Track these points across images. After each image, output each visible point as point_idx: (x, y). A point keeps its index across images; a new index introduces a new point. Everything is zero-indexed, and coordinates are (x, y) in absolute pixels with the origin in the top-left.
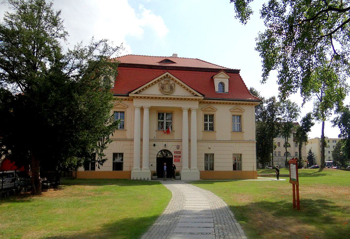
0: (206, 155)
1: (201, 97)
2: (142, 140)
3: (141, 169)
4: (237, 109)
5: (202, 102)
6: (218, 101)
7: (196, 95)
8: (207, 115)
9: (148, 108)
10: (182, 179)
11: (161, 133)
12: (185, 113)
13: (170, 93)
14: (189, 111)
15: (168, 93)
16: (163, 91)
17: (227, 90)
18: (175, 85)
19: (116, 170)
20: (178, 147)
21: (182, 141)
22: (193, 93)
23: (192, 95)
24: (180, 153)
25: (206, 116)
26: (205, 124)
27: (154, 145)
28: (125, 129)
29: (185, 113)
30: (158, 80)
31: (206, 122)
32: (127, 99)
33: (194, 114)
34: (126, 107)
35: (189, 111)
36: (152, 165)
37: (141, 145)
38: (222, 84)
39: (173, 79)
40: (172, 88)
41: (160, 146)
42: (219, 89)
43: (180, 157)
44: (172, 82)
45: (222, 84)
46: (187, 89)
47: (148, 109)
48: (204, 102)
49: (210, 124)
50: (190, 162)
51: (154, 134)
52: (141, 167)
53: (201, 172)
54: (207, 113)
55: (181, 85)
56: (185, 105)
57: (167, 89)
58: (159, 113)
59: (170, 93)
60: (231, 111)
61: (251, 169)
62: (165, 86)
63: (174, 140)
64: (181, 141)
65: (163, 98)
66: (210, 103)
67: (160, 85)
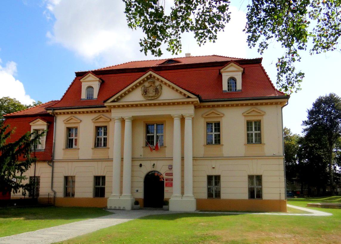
0: (210, 178)
1: (196, 100)
4: (212, 114)
6: (246, 101)
7: (189, 97)
8: (252, 122)
9: (129, 119)
11: (148, 149)
12: (177, 123)
13: (156, 98)
14: (183, 119)
15: (153, 98)
16: (146, 96)
17: (239, 87)
18: (162, 87)
19: (100, 197)
20: (171, 167)
21: (172, 160)
22: (185, 95)
23: (182, 97)
27: (141, 165)
28: (221, 144)
29: (177, 123)
30: (140, 83)
33: (188, 123)
34: (79, 121)
35: (183, 119)
36: (137, 191)
37: (122, 166)
38: (233, 79)
39: (158, 79)
40: (157, 91)
41: (148, 168)
42: (228, 86)
45: (232, 80)
46: (177, 90)
47: (191, 119)
48: (204, 107)
50: (183, 187)
51: (202, 151)
52: (121, 193)
54: (250, 119)
55: (169, 86)
56: (175, 112)
57: (151, 92)
58: (146, 124)
59: (156, 98)
60: (244, 116)
61: (276, 197)
62: (148, 90)
64: (171, 159)
65: (146, 105)
66: (213, 106)
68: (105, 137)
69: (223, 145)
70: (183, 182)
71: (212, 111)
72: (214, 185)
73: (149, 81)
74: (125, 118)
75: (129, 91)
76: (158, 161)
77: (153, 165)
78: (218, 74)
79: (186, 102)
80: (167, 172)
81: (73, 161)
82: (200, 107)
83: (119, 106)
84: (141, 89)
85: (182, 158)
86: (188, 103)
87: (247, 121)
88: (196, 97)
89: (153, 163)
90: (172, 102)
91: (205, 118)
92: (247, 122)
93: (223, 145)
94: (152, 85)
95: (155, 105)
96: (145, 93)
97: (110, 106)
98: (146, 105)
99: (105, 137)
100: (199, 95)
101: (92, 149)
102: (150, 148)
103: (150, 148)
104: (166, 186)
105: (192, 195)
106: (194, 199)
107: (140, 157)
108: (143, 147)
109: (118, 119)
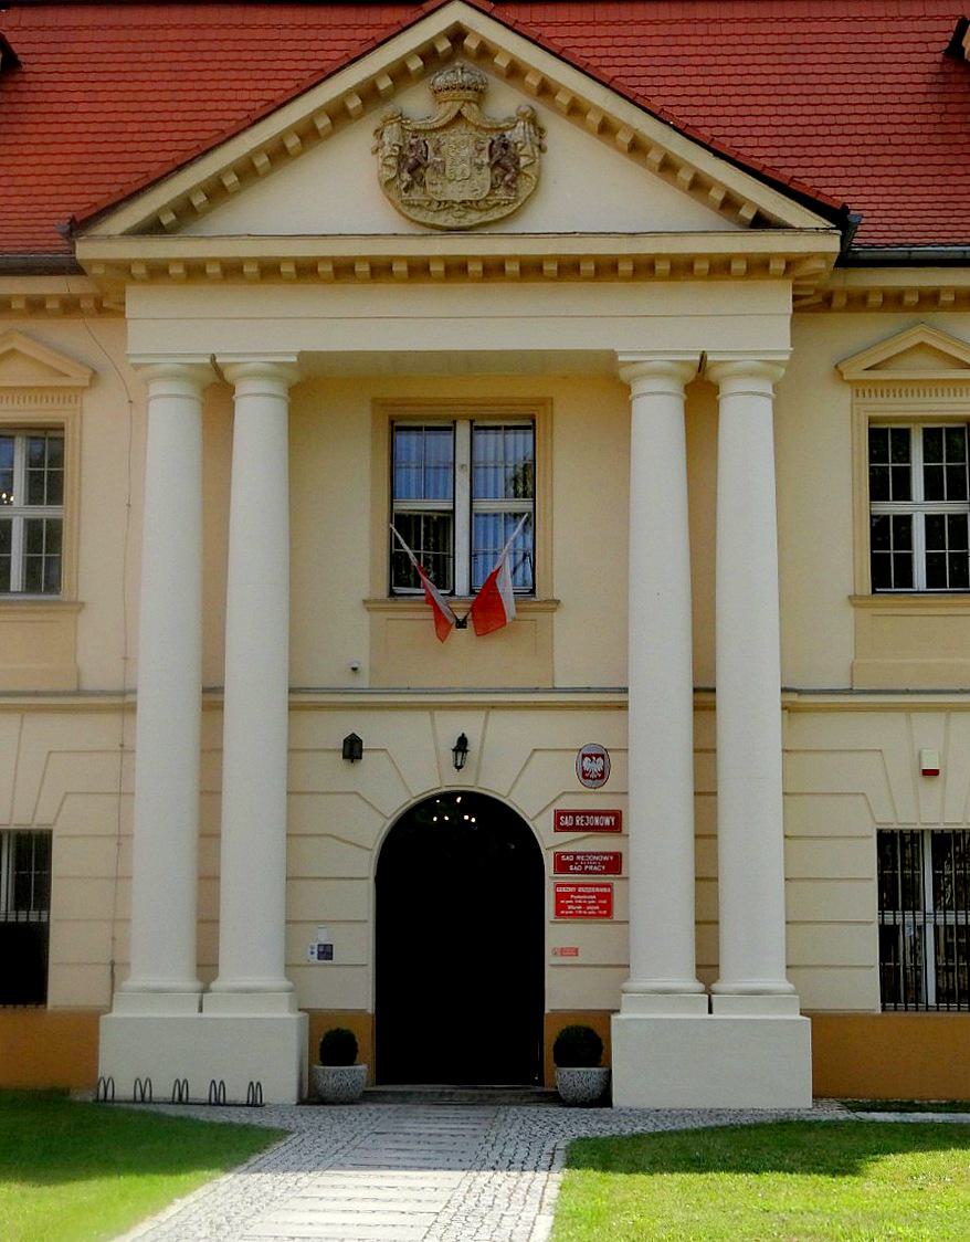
1: (818, 241)
2: (212, 698)
3: (709, 992)
4: (920, 359)
5: (839, 301)
7: (762, 222)
9: (668, 374)
10: (615, 1100)
11: (413, 621)
13: (496, 214)
15: (474, 218)
16: (416, 195)
18: (541, 131)
20: (596, 766)
21: (623, 707)
22: (730, 204)
23: (710, 218)
24: (615, 823)
25: (886, 443)
26: (56, 497)
27: (352, 749)
30: (370, 94)
31: (892, 508)
32: (87, 304)
34: (79, 378)
36: (326, 952)
37: (211, 750)
39: (515, 72)
43: (614, 864)
44: (506, 103)
46: (668, 167)
48: (858, 302)
49: (933, 522)
50: (707, 924)
52: (206, 968)
53: (828, 1030)
55: (606, 129)
59: (496, 214)
62: (437, 151)
63: (554, 690)
64: (614, 701)
65: (419, 270)
66: (930, 299)
67: (392, 135)
68: (44, 512)
69: (80, 606)
70: (706, 880)
71: (916, 341)
72: (929, 906)
73: (440, 81)
74: (240, 369)
75: (278, 154)
76: (495, 716)
77: (456, 750)
78: (939, 57)
79: (512, 258)
80: (563, 805)
81: (494, 706)
82: (826, 302)
83: (195, 271)
84: (372, 142)
85: (205, 691)
86: (758, 267)
87: (871, 420)
88: (821, 222)
89: (452, 726)
90: (332, 259)
91: (858, 387)
92: (872, 432)
93: (555, 604)
94: (465, 112)
95: (494, 269)
96: (406, 176)
97: (124, 269)
98: (419, 270)
99: (44, 512)
100: (845, 209)
101: (854, 600)
102: (437, 609)
103: (431, 615)
104: (558, 914)
105: (779, 982)
106: (296, 1016)
107: (347, 681)
108: (370, 605)
109: (268, 368)
